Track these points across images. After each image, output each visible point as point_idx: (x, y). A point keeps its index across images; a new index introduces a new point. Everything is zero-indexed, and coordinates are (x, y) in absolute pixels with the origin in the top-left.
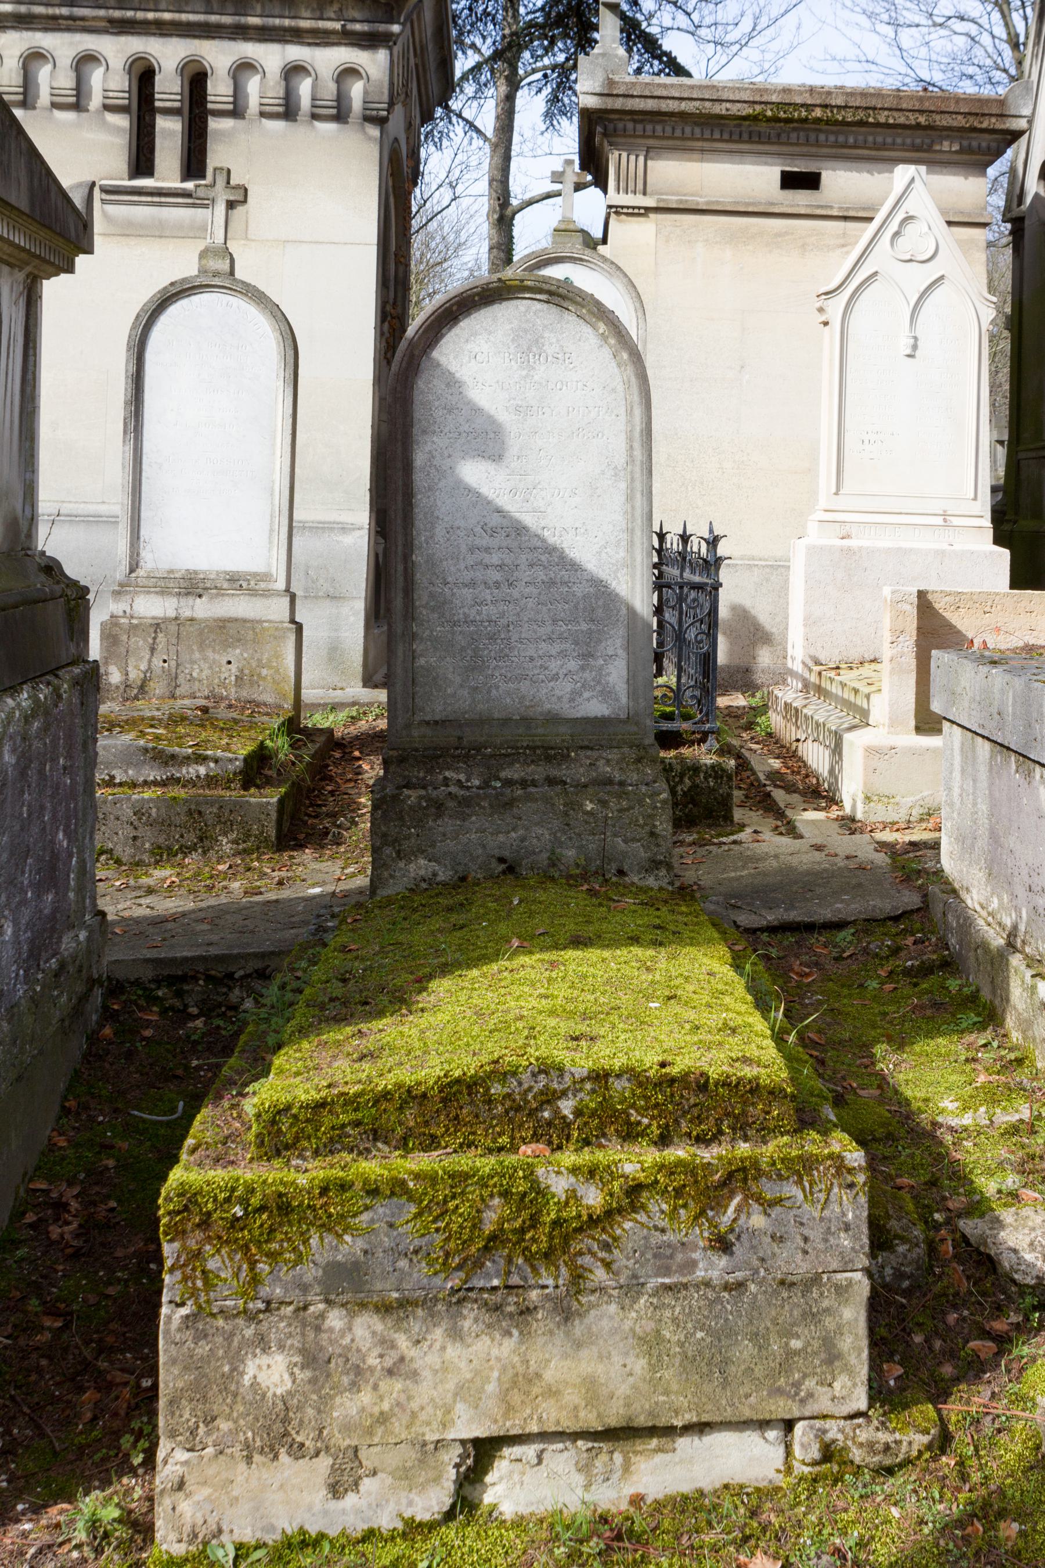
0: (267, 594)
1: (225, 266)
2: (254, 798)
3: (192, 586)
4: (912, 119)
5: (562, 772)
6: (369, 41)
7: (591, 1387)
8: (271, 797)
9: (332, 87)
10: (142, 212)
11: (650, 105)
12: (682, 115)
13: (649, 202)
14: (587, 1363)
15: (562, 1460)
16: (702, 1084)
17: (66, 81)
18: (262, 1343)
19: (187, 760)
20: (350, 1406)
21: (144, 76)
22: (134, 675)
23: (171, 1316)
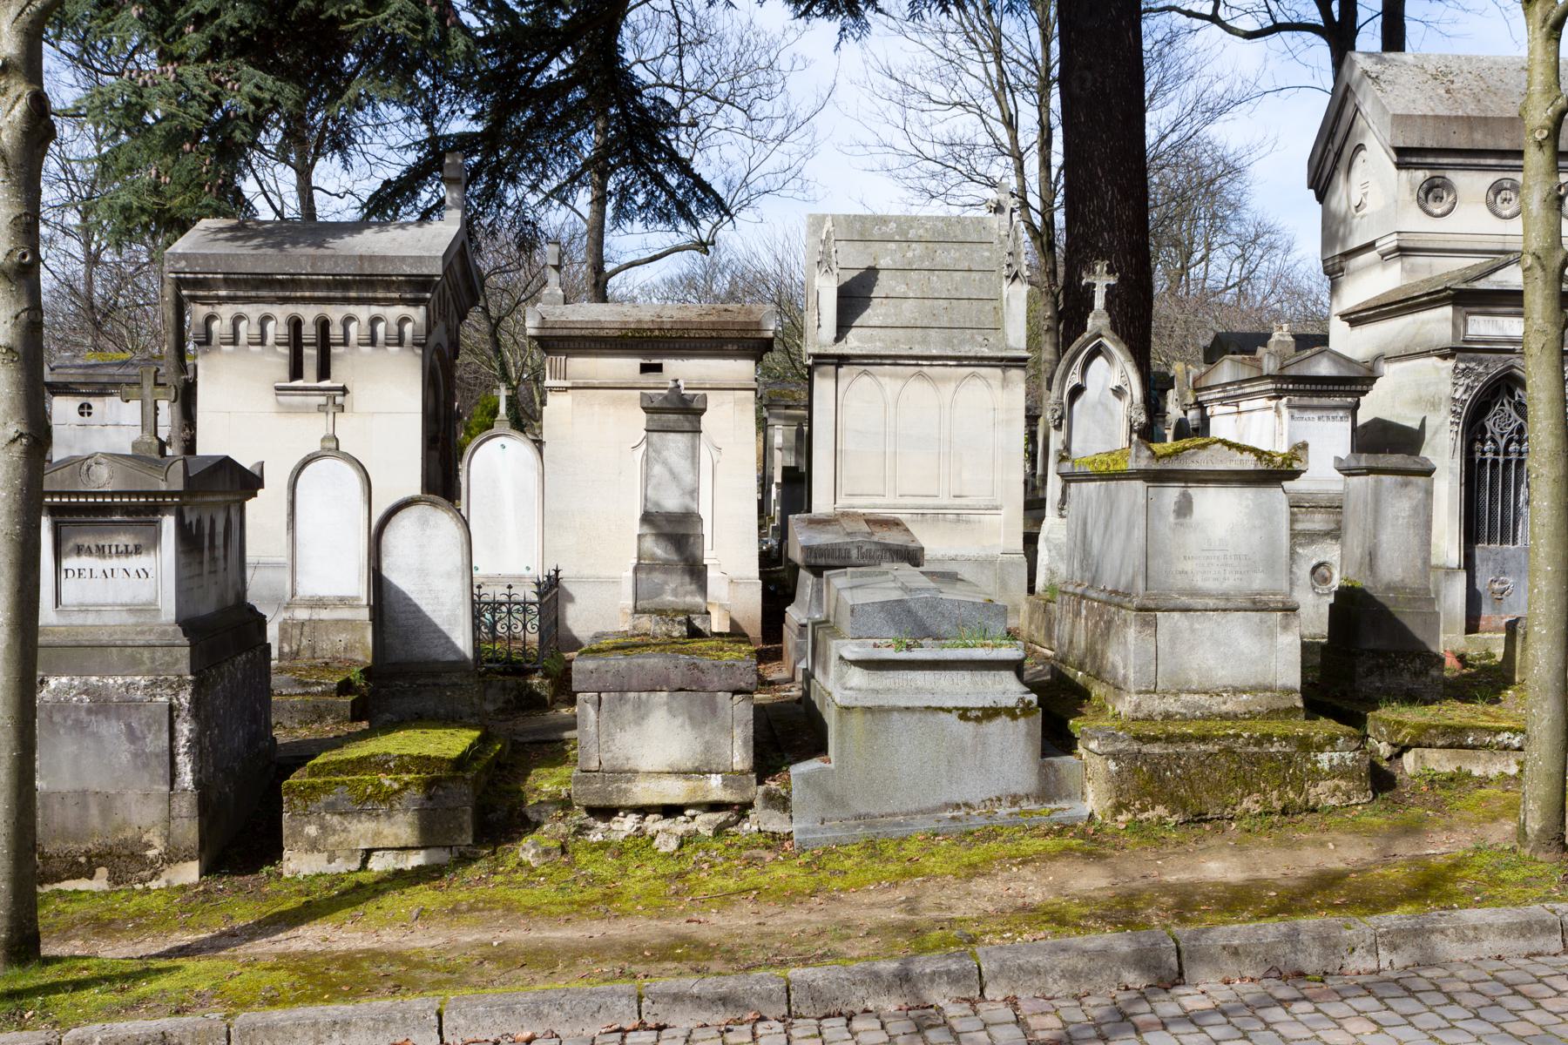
0: (358, 607)
1: (333, 445)
2: (342, 700)
3: (318, 603)
4: (709, 334)
5: (439, 681)
6: (415, 302)
7: (396, 836)
8: (349, 699)
9: (396, 328)
10: (297, 399)
11: (565, 332)
12: (583, 337)
13: (568, 384)
14: (395, 830)
15: (390, 856)
16: (428, 758)
17: (256, 331)
18: (309, 823)
19: (313, 684)
20: (332, 839)
21: (296, 324)
22: (295, 648)
23: (285, 816)
